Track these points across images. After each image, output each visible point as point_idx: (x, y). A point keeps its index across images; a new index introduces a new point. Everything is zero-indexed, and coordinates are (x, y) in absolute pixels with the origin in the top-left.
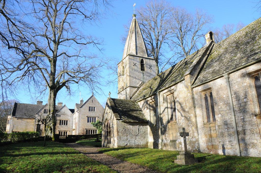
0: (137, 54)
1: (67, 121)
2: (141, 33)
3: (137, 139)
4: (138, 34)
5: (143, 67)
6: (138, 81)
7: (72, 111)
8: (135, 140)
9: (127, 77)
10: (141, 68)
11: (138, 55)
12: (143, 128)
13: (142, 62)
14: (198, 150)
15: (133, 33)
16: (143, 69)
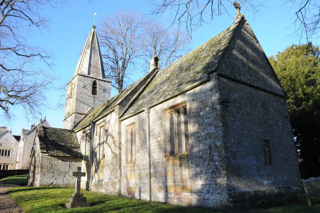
0: (89, 73)
1: (9, 151)
3: (66, 177)
4: (94, 50)
5: (95, 90)
6: (86, 107)
7: (18, 138)
8: (64, 178)
10: (93, 91)
11: (90, 76)
12: (75, 164)
13: (94, 84)
14: (119, 192)
15: (88, 48)
16: (94, 92)
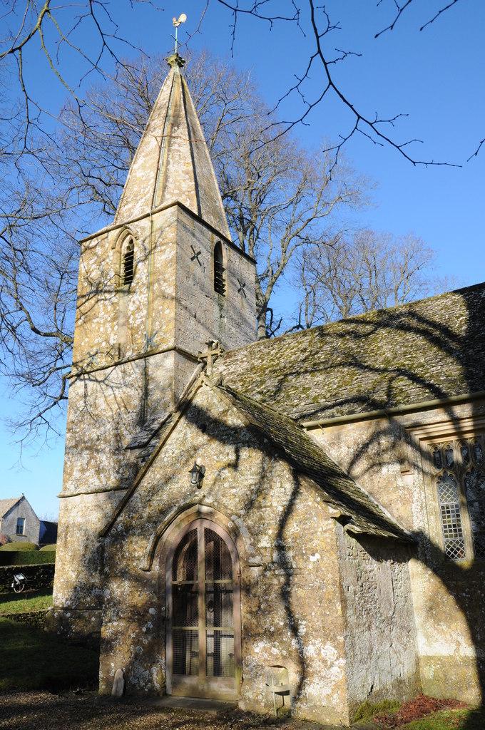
2: (99, 232)
9: (157, 304)
16: (219, 287)
